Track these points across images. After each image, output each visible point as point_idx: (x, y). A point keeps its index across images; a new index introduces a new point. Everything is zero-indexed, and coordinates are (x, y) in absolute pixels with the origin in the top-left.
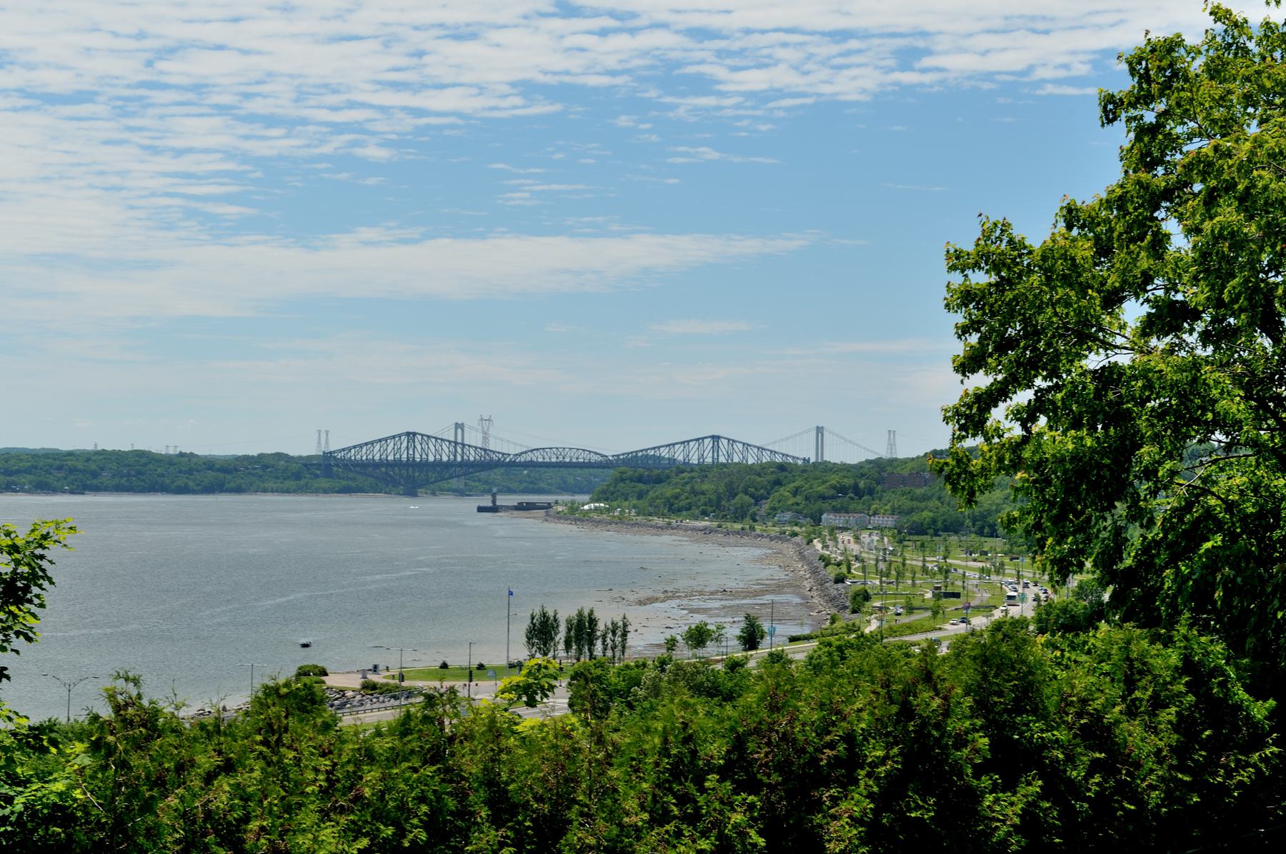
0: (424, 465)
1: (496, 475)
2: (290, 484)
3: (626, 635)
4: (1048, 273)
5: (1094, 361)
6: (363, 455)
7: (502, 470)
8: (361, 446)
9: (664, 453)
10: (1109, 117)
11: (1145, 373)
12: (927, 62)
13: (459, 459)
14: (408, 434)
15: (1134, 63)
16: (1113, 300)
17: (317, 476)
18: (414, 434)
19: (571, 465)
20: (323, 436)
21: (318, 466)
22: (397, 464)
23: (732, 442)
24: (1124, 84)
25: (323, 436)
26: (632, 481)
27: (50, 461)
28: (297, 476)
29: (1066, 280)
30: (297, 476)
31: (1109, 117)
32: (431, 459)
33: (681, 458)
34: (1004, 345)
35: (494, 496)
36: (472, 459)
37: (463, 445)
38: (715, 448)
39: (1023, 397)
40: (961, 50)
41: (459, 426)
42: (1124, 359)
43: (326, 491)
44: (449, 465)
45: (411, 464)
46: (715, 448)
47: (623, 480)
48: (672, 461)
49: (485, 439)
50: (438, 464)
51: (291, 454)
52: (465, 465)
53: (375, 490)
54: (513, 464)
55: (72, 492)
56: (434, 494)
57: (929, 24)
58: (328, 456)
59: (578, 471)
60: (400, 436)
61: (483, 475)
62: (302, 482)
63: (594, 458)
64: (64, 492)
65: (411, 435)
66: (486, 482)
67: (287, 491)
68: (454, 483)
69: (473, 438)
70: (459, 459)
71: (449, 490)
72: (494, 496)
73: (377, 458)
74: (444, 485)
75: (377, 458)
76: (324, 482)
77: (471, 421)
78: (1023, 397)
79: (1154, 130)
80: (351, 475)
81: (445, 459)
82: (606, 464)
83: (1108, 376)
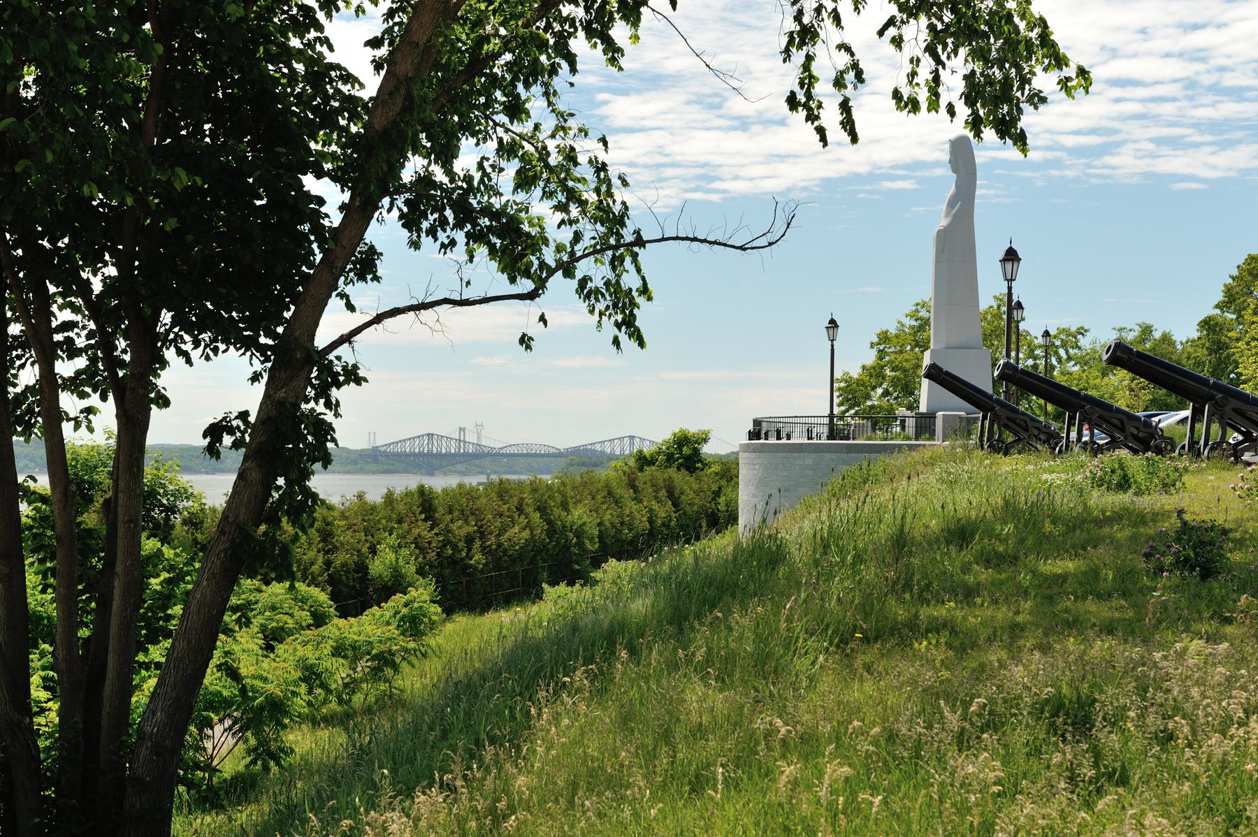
0: (439, 455)
1: (486, 462)
2: (350, 467)
3: (354, 647)
4: (858, 385)
5: (869, 403)
6: (399, 449)
7: (489, 458)
8: (397, 443)
9: (598, 447)
10: (872, 347)
11: (880, 407)
12: (717, 185)
13: (462, 451)
14: (428, 435)
15: (879, 336)
16: (874, 388)
17: (368, 462)
18: (433, 435)
19: (535, 455)
20: (372, 436)
21: (369, 456)
22: (421, 454)
23: (642, 440)
24: (876, 340)
25: (372, 436)
26: (578, 465)
27: (191, 453)
28: (355, 462)
29: (862, 385)
30: (355, 462)
31: (872, 347)
32: (444, 451)
33: (609, 451)
34: (848, 400)
35: (488, 475)
36: (444, 451)
37: (465, 442)
38: (632, 444)
39: (852, 412)
40: (736, 178)
41: (462, 430)
42: (876, 403)
43: (374, 473)
44: (455, 455)
45: (430, 455)
46: (632, 444)
47: (572, 465)
48: (603, 453)
49: (479, 438)
50: (448, 455)
51: (351, 447)
52: (465, 455)
53: (407, 472)
54: (497, 455)
55: (207, 473)
56: (445, 474)
57: (715, 159)
58: (375, 449)
59: (540, 459)
60: (423, 436)
61: (477, 462)
62: (359, 466)
63: (552, 451)
64: (201, 473)
65: (430, 436)
66: (480, 467)
67: (349, 472)
68: (459, 467)
69: (471, 437)
70: (462, 451)
71: (455, 472)
72: (488, 475)
73: (408, 450)
74: (452, 468)
75: (408, 450)
76: (373, 467)
77: (470, 426)
78: (852, 412)
79: (882, 351)
80: (391, 462)
81: (453, 451)
82: (559, 455)
83: (872, 407)
